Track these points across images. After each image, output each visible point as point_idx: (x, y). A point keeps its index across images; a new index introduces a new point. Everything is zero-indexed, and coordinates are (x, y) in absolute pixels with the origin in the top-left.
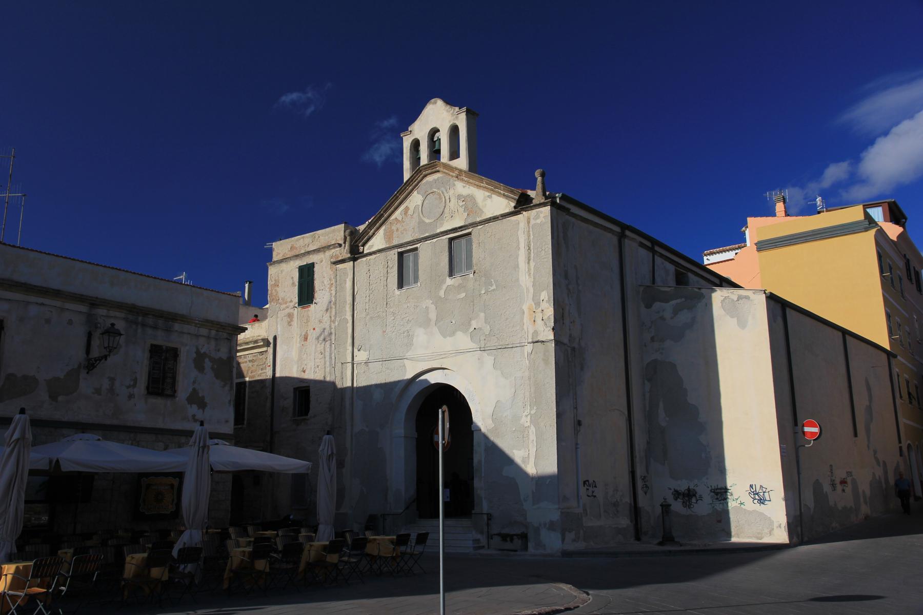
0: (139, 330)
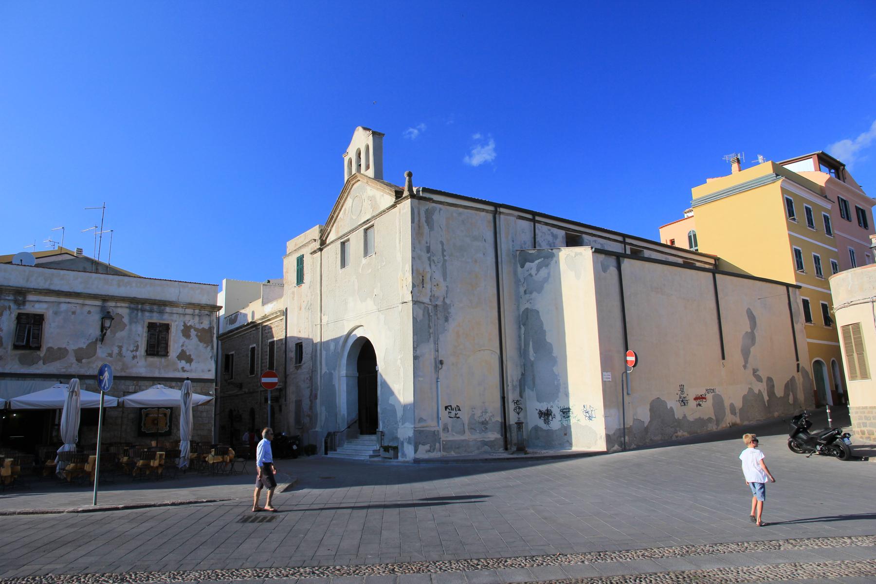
0: (140, 314)
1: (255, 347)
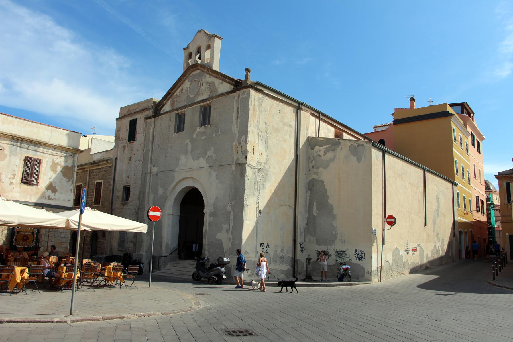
1: (81, 185)
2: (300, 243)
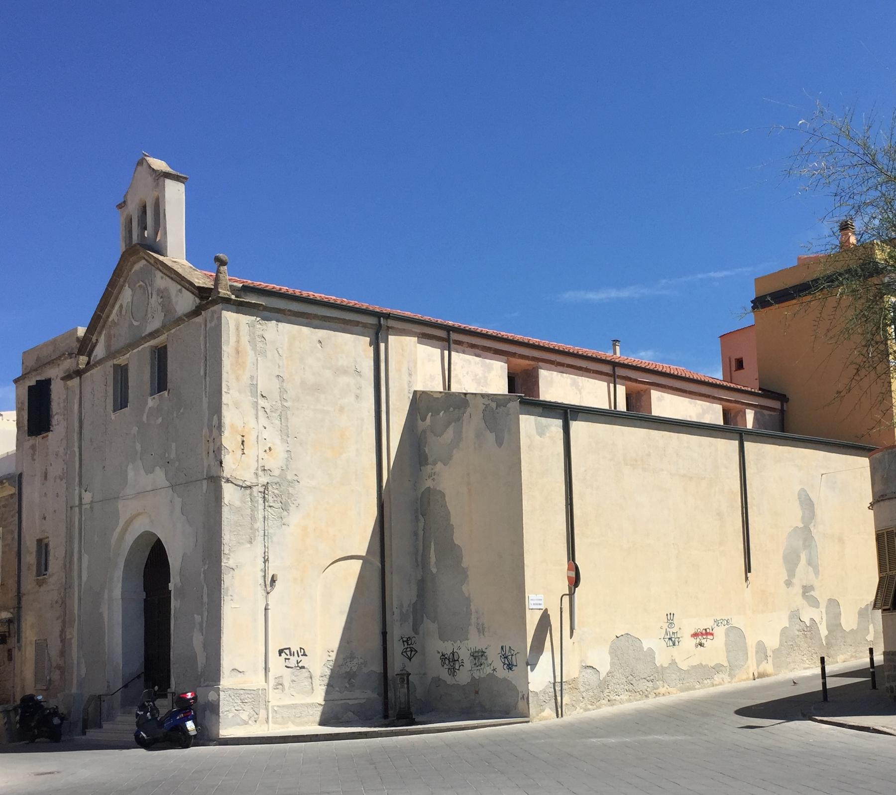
2: (402, 638)
